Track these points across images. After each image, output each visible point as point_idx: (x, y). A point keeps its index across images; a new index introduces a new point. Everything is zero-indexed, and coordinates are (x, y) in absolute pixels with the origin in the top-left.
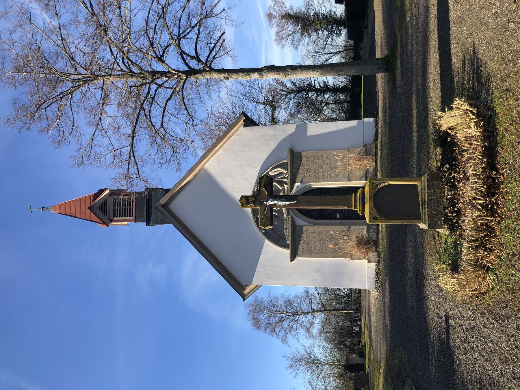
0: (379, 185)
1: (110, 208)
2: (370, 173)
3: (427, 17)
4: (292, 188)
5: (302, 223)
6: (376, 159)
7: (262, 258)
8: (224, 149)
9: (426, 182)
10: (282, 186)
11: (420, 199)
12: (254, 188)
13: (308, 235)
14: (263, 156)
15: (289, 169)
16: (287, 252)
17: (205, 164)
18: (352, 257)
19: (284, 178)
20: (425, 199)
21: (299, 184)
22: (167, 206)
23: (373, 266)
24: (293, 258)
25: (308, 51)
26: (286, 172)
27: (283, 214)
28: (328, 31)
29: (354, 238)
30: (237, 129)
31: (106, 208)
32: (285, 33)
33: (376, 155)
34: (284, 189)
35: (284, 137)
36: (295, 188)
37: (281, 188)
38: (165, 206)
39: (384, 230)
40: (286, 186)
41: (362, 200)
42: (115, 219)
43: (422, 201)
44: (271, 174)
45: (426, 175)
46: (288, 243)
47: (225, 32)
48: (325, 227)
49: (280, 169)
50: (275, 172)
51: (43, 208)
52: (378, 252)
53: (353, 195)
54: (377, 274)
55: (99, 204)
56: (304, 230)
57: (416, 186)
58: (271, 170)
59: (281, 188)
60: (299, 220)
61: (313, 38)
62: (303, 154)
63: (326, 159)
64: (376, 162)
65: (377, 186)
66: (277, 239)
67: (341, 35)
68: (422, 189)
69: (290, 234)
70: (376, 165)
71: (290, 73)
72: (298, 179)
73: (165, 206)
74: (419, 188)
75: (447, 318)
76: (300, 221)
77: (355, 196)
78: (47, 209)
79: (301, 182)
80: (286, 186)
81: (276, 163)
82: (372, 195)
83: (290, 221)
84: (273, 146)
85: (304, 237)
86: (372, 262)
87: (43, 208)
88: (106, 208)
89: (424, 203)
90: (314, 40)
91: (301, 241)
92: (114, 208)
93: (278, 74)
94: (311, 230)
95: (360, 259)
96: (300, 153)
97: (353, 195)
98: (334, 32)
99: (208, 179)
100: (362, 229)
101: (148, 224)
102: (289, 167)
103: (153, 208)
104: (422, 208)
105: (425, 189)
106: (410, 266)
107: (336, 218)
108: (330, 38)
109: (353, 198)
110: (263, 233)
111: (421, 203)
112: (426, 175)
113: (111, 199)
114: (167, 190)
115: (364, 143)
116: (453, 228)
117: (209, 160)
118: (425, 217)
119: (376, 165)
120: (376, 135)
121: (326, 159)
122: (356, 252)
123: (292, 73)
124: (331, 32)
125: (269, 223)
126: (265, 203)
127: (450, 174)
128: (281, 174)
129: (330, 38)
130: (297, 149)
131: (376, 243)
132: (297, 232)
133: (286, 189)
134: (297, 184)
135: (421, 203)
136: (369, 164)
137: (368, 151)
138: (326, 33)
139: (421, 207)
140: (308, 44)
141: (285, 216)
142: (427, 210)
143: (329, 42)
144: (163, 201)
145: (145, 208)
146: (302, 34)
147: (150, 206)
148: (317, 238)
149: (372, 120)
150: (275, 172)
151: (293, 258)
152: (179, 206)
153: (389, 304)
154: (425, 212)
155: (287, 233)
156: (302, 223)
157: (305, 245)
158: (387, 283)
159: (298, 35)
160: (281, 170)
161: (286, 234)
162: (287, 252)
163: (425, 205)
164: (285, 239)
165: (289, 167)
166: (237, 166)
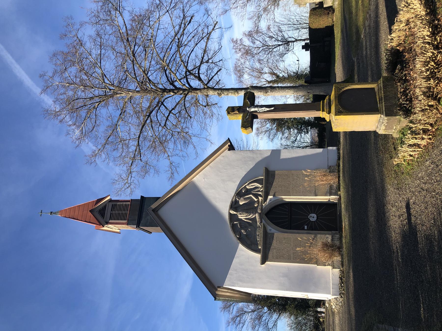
0: (343, 88)
1: (108, 212)
2: (333, 190)
3: (377, 16)
4: (265, 199)
5: (273, 231)
6: (339, 174)
7: (235, 261)
8: (211, 167)
9: (382, 84)
10: (257, 197)
11: (377, 97)
12: (233, 198)
13: (278, 242)
14: (243, 173)
15: (264, 184)
16: (258, 256)
17: (194, 177)
18: (317, 263)
19: (259, 191)
20: (381, 96)
21: (272, 197)
22: (157, 211)
23: (337, 271)
24: (263, 262)
25: (281, 144)
26: (261, 186)
27: (256, 222)
28: (298, 129)
29: (320, 244)
30: (223, 152)
31: (104, 212)
32: (264, 129)
33: (339, 171)
34: (258, 201)
35: (260, 159)
36: (268, 201)
37: (256, 200)
38: (155, 211)
39: (347, 227)
40: (260, 198)
41: (328, 104)
42: (110, 221)
43: (379, 98)
44: (248, 187)
45: (381, 79)
46: (260, 248)
47: (221, 69)
48: (293, 235)
49: (256, 184)
50: (252, 186)
51: (51, 212)
52: (342, 256)
53: (321, 102)
54: (341, 278)
55: (100, 208)
56: (275, 237)
57: (374, 88)
58: (248, 184)
59: (256, 200)
60: (270, 228)
61: (286, 135)
62: (277, 172)
63: (295, 177)
64: (339, 177)
65: (341, 89)
66: (251, 245)
67: (308, 133)
68: (378, 90)
69: (262, 239)
70: (339, 180)
71: (269, 91)
72: (272, 192)
73: (155, 211)
74: (376, 90)
75: (408, 206)
76: (271, 229)
77: (323, 103)
78: (55, 213)
79: (274, 196)
80: (260, 198)
81: (253, 179)
82: (337, 95)
83: (262, 228)
84: (251, 165)
85: (275, 244)
86: (336, 268)
87: (51, 212)
88: (104, 212)
89: (381, 99)
90: (286, 136)
91: (272, 247)
92: (112, 212)
93: (260, 92)
94: (282, 238)
95: (326, 265)
96: (274, 172)
97: (321, 102)
98: (302, 130)
99: (195, 192)
100: (327, 238)
101: (138, 226)
102: (264, 182)
103: (144, 213)
104: (380, 103)
105: (381, 89)
106: (372, 219)
107: (303, 229)
108: (300, 135)
109: (321, 104)
110: (237, 238)
111: (378, 100)
112: (381, 79)
113: (111, 204)
114: (158, 198)
115: (328, 166)
116: (407, 112)
117: (197, 174)
118: (382, 109)
119: (339, 180)
120: (339, 159)
121: (295, 177)
122: (322, 256)
123: (271, 91)
124: (300, 131)
125: (249, 125)
126: (248, 109)
127: (402, 73)
128: (256, 188)
129: (300, 135)
130: (271, 169)
131: (340, 248)
132: (268, 239)
133: (260, 200)
134: (270, 197)
135: (378, 100)
136: (332, 180)
137: (332, 170)
138: (296, 131)
139: (378, 103)
140: (281, 139)
141: (258, 224)
142: (383, 104)
143: (298, 138)
144: (154, 206)
145: (137, 213)
146: (277, 130)
147: (142, 213)
148: (286, 244)
149: (335, 148)
150: (252, 186)
151: (263, 262)
152: (166, 213)
153: (352, 291)
154: (382, 105)
155: (260, 239)
156: (273, 231)
157: (275, 250)
158: (351, 271)
159: (274, 131)
160: (257, 185)
161: (258, 240)
162: (258, 256)
163: (382, 100)
164: (257, 245)
165: (264, 182)
166: (219, 186)
